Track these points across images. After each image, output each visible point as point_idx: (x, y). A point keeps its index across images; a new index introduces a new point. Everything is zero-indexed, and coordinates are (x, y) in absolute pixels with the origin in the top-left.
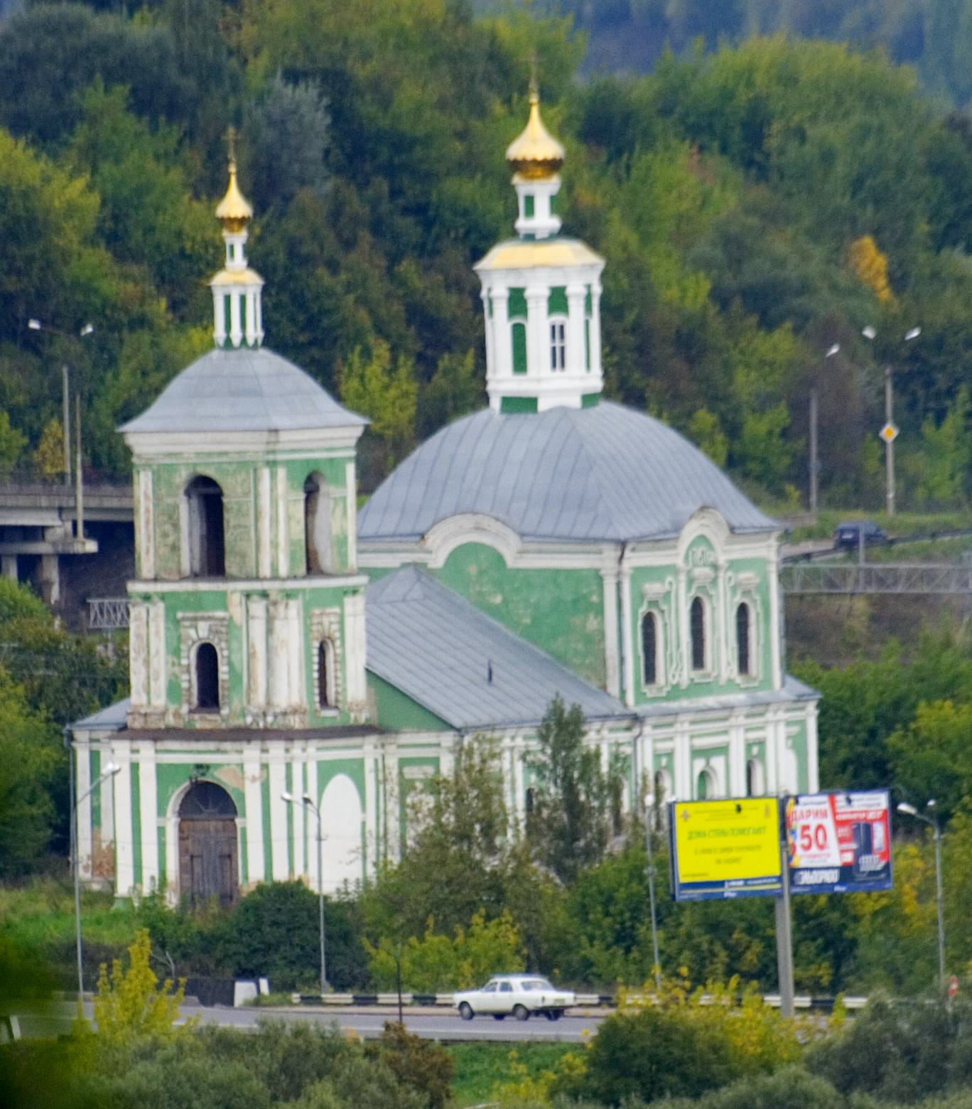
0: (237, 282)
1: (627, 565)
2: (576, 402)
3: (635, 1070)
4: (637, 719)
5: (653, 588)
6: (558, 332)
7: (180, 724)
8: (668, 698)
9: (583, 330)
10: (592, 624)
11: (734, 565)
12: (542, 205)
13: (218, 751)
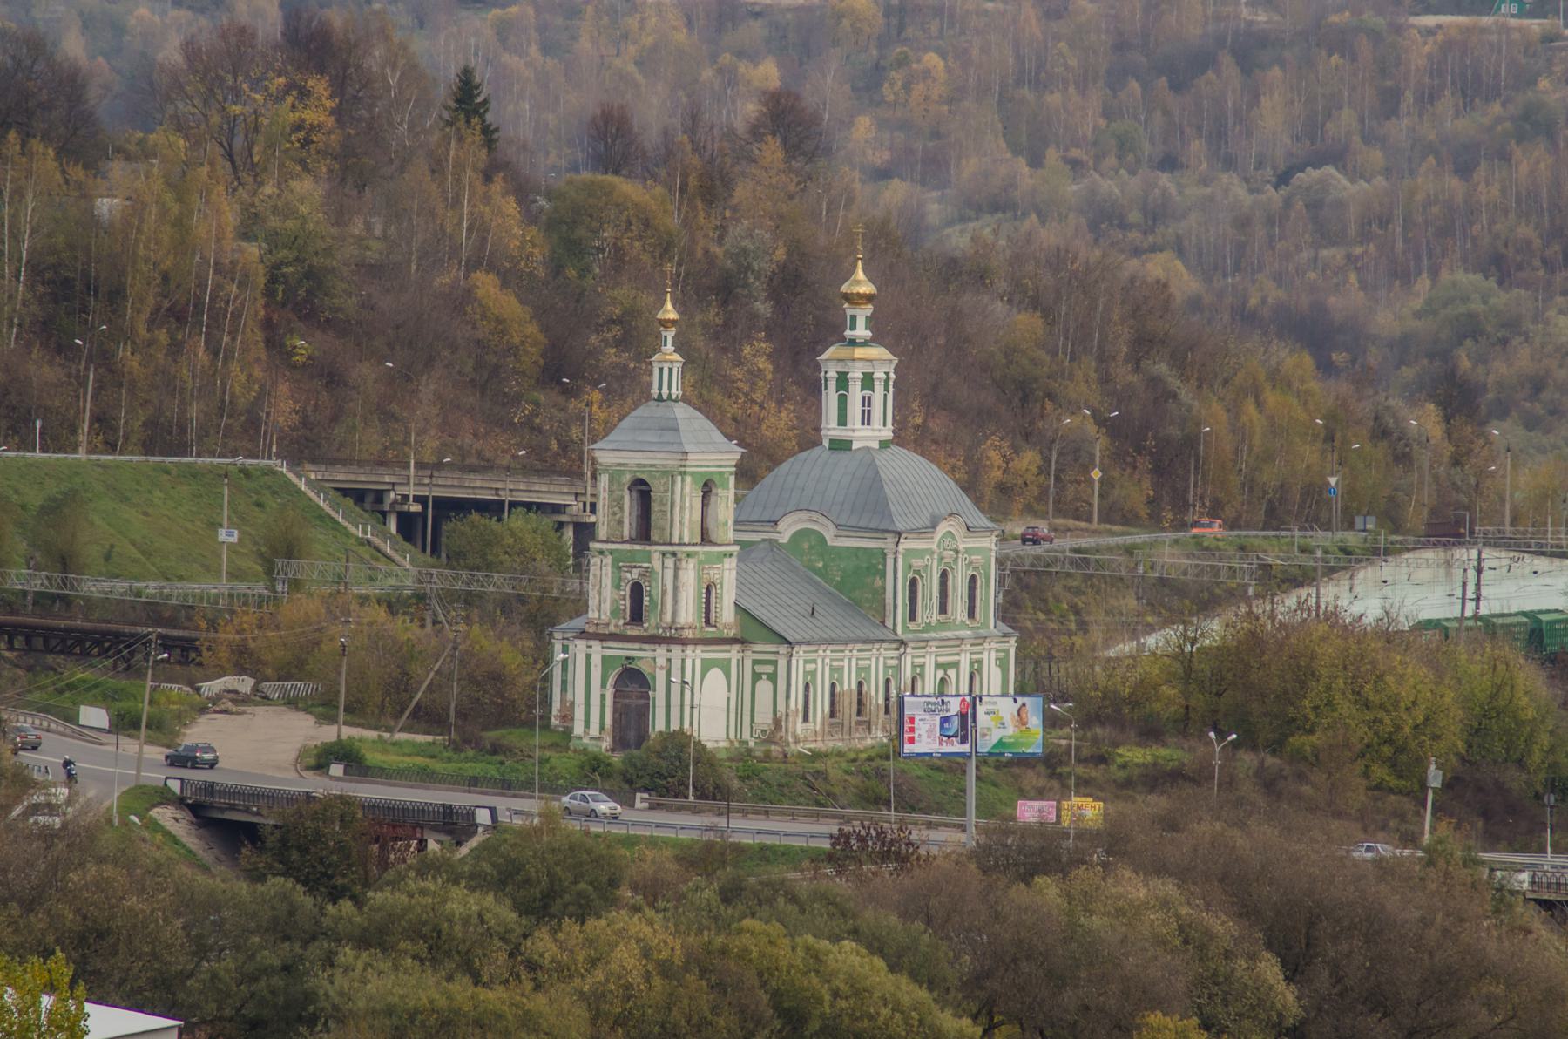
6: (867, 401)
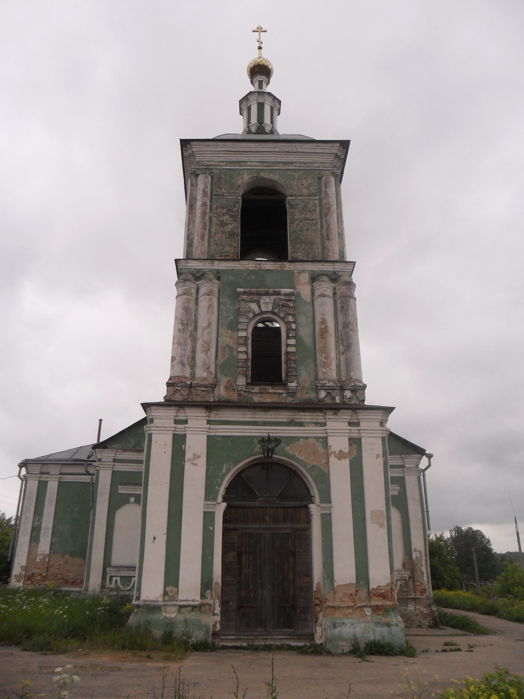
3: (158, 633)
7: (234, 397)
13: (292, 423)
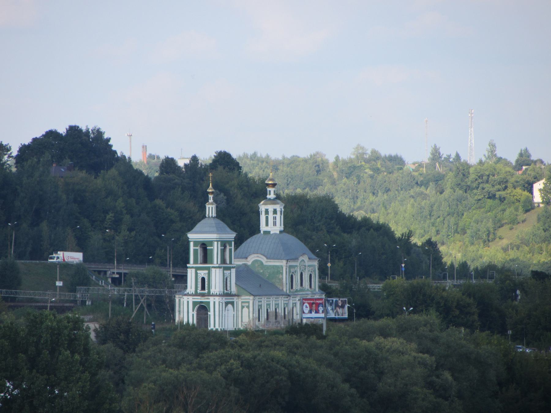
0: (211, 209)
1: (288, 265)
2: (278, 232)
4: (289, 295)
5: (292, 270)
6: (275, 218)
8: (296, 292)
9: (279, 218)
10: (281, 276)
11: (309, 266)
12: (272, 193)
